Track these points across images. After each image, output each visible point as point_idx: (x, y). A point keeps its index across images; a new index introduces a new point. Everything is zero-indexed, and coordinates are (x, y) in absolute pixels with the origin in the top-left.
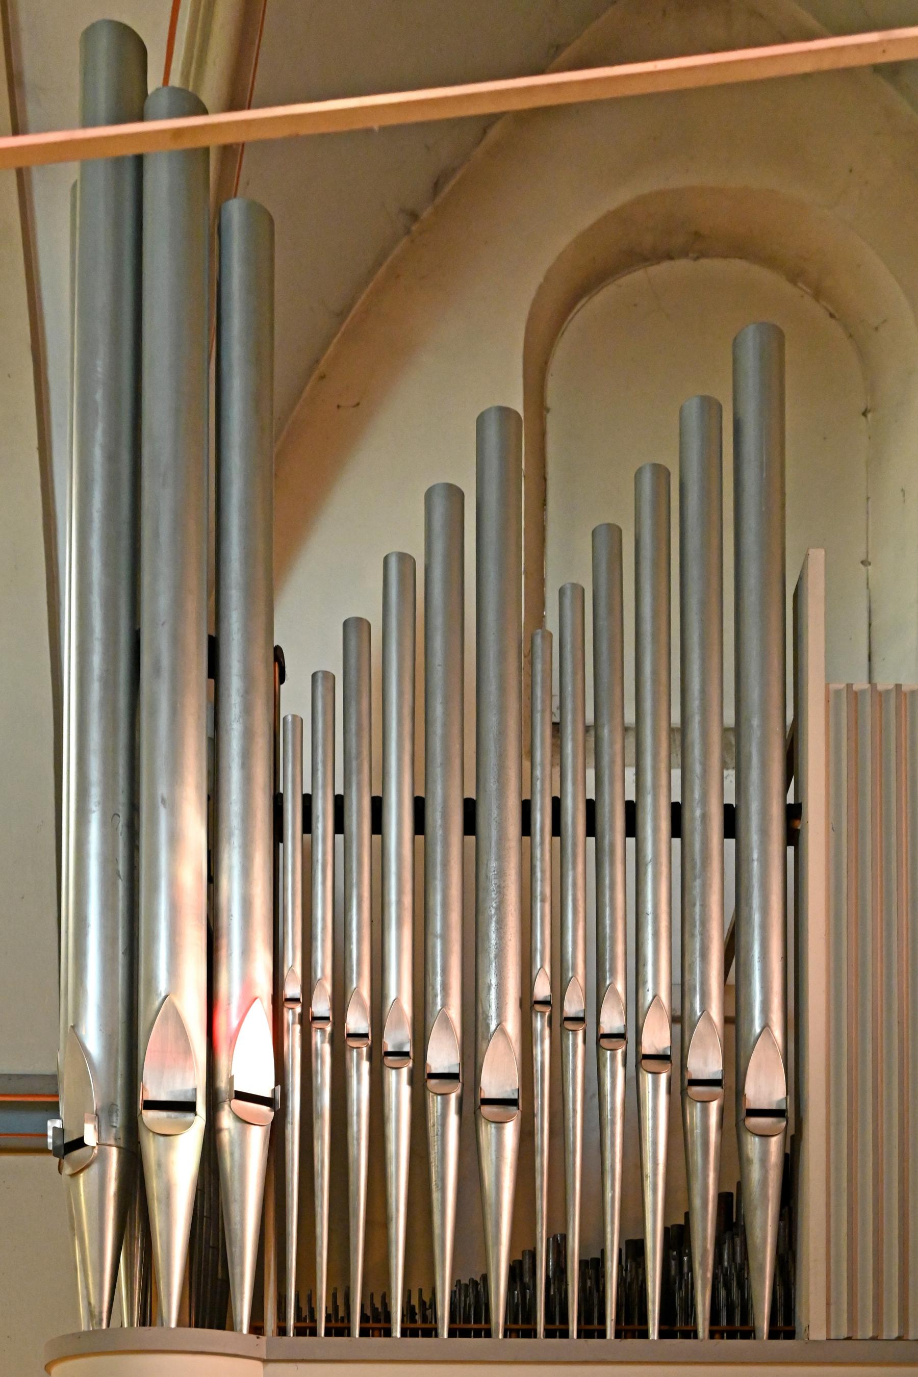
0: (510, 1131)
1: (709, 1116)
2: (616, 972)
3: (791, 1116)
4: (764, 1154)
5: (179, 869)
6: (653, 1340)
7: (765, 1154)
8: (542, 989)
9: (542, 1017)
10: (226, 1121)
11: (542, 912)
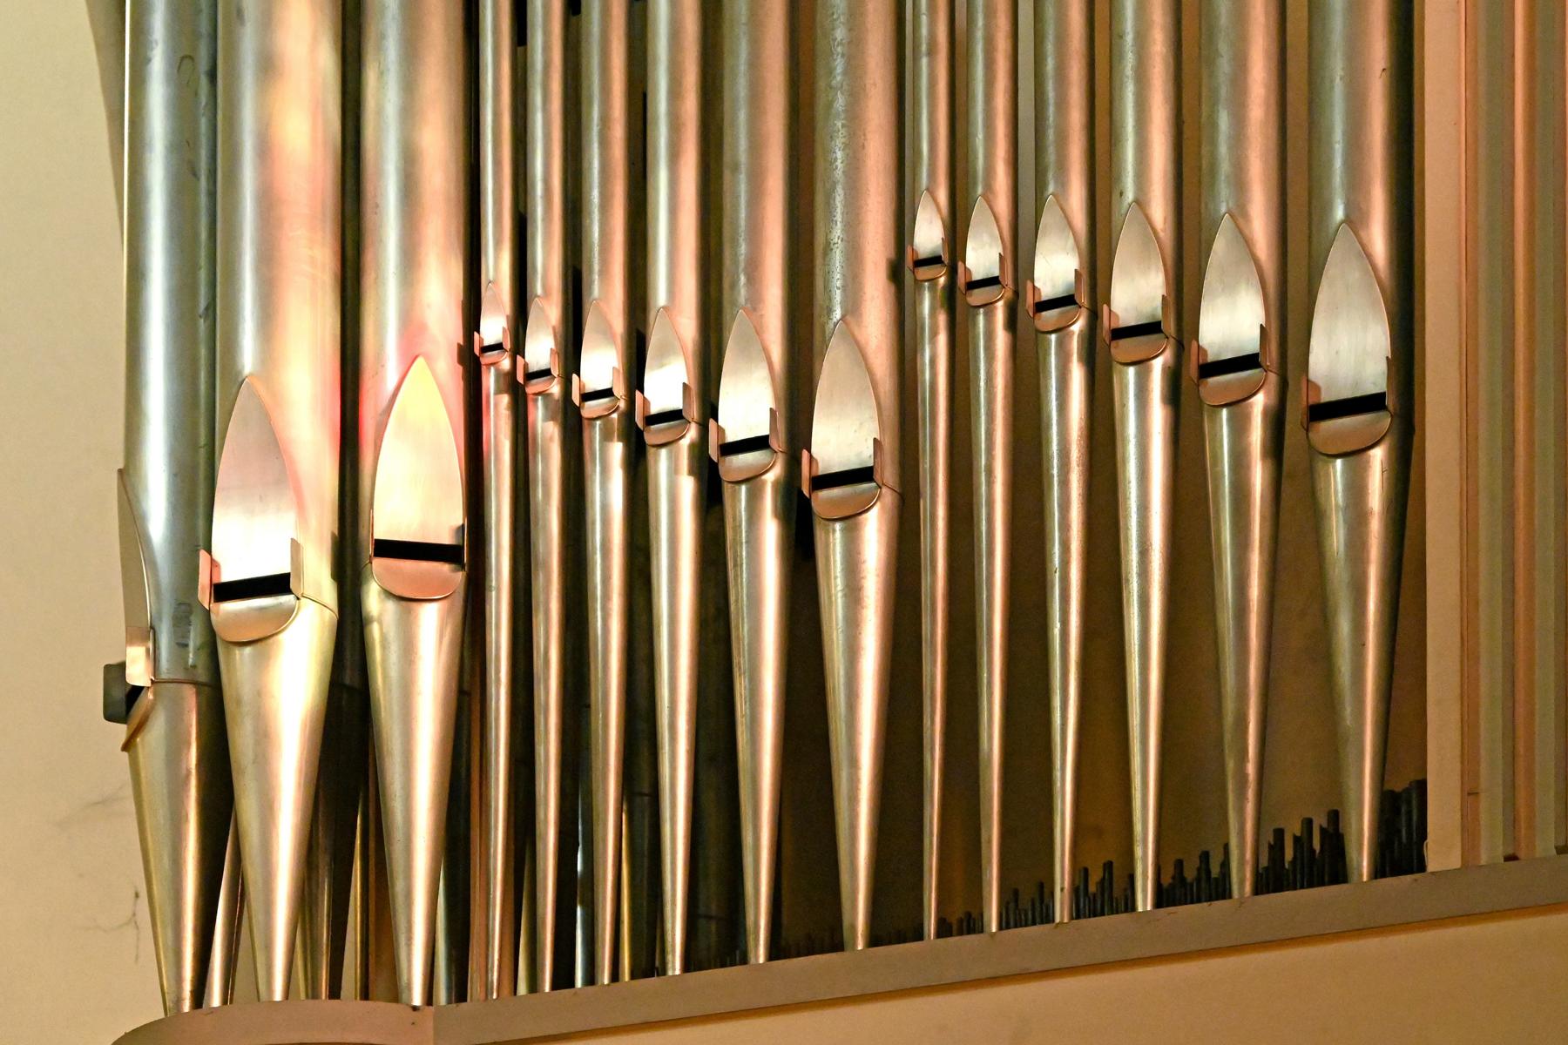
0: (874, 530)
1: (1242, 437)
2: (995, 12)
3: (1399, 404)
4: (1356, 485)
5: (291, 120)
6: (1145, 912)
7: (1357, 489)
8: (928, 235)
9: (933, 288)
10: (374, 600)
11: (932, 75)
